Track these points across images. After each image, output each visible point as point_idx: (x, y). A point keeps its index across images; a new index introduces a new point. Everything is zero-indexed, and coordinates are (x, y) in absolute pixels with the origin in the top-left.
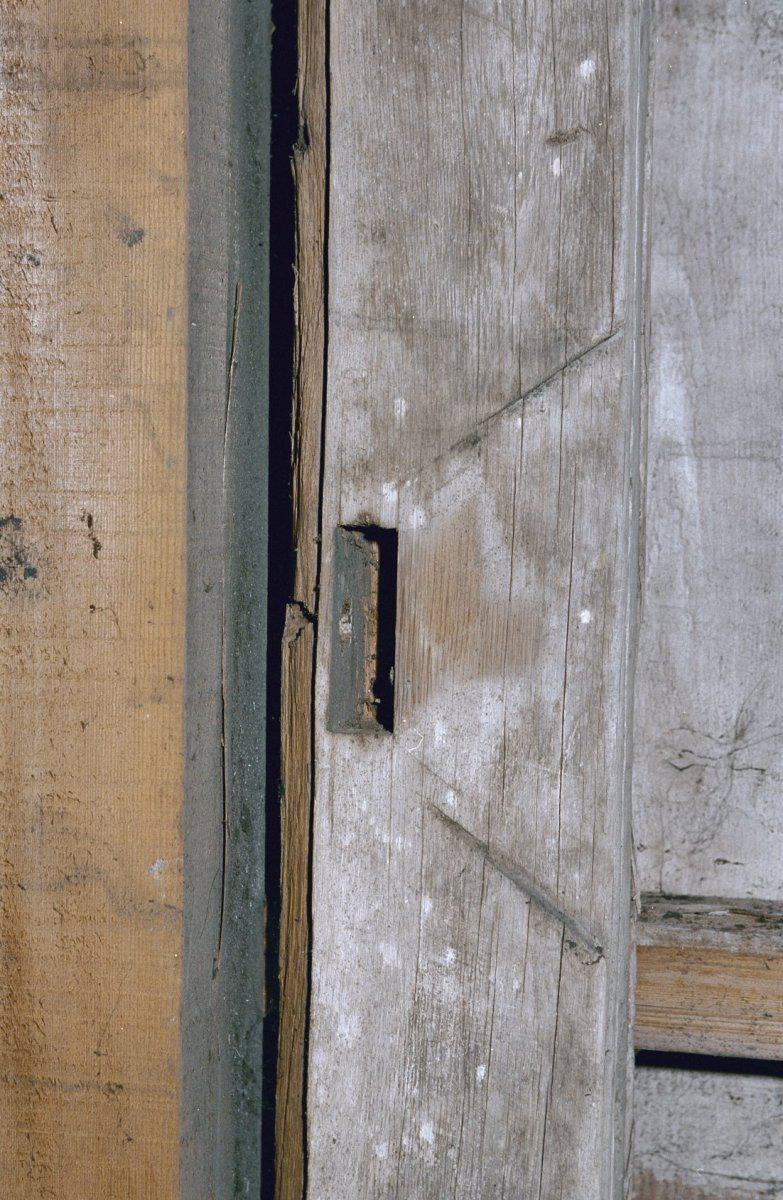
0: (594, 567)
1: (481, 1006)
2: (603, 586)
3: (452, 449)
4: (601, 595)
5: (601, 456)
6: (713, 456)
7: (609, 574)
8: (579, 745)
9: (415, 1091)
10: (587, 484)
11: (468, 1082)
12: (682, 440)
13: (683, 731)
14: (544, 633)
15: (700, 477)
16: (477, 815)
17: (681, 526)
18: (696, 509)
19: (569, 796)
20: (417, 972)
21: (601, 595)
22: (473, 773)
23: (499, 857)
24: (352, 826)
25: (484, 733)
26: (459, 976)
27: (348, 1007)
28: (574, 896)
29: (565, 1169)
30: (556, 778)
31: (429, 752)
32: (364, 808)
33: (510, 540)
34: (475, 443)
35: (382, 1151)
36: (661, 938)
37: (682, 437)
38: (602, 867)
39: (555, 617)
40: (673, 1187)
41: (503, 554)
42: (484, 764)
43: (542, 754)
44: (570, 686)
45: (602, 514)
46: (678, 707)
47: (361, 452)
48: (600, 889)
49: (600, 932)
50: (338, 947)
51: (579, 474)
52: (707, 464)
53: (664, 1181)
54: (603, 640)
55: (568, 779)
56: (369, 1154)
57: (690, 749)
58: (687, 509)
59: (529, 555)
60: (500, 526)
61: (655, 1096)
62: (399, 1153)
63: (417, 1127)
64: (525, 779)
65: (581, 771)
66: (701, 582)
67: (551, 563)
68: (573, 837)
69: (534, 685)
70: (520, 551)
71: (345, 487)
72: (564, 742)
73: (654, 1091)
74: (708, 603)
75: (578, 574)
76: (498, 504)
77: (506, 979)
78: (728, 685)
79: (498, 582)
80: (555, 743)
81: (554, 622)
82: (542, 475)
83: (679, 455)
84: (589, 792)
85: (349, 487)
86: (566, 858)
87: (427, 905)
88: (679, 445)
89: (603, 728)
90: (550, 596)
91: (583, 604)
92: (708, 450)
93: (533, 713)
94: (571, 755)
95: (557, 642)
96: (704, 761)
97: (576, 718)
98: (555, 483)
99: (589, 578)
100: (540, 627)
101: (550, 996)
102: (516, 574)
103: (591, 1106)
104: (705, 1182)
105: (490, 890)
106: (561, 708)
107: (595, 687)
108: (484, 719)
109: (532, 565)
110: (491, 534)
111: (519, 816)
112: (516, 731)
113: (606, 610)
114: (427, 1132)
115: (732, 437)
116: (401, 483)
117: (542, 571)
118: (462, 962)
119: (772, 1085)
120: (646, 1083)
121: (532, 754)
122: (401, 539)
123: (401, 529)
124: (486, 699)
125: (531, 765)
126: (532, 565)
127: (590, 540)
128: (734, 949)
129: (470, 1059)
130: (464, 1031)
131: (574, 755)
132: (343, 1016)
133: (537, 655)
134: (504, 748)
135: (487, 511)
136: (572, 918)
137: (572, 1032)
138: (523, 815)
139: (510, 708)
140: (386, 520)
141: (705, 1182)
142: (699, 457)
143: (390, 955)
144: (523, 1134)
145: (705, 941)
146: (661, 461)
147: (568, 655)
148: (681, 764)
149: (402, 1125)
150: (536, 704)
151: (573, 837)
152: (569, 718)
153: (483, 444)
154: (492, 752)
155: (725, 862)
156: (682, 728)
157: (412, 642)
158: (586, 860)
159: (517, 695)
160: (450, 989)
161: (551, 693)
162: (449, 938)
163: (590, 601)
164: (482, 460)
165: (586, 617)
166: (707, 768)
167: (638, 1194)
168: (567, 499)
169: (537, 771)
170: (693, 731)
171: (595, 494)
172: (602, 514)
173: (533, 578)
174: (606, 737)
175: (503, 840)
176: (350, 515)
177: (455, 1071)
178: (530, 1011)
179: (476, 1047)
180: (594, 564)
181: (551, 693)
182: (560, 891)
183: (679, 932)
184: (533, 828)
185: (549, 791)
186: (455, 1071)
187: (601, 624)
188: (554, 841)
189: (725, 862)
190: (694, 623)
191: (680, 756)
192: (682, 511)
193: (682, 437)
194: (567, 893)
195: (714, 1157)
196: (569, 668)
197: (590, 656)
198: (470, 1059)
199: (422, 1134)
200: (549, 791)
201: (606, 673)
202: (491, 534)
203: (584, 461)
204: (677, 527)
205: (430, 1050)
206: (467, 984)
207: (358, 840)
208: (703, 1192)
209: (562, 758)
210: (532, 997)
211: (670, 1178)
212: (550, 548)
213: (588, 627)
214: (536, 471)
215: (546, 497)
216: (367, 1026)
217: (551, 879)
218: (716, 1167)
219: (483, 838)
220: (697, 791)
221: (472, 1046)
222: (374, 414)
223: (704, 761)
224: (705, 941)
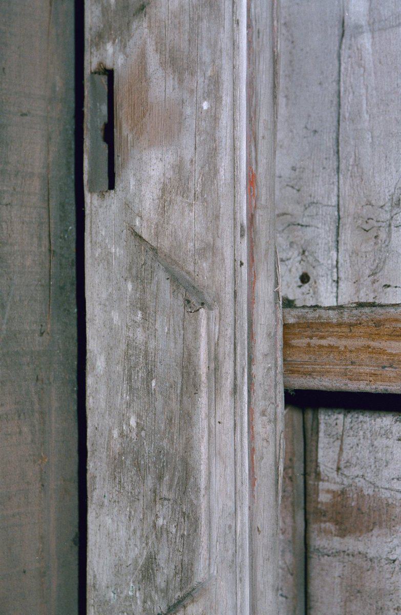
0: (209, 75)
1: (152, 345)
2: (214, 85)
3: (134, 15)
4: (213, 91)
5: (211, 6)
6: (379, 29)
7: (218, 78)
8: (203, 185)
9: (128, 397)
10: (204, 25)
11: (149, 391)
12: (363, 23)
13: (368, 206)
14: (184, 118)
15: (373, 44)
16: (150, 230)
17: (364, 78)
18: (371, 65)
19: (199, 216)
20: (127, 327)
21: (213, 91)
22: (148, 205)
23: (163, 256)
24: (99, 245)
25: (152, 181)
26: (143, 327)
27: (100, 350)
28: (203, 277)
29: (189, 440)
30: (192, 205)
31: (128, 196)
32: (103, 233)
33: (162, 64)
34: (143, 9)
35: (115, 433)
36: (298, 317)
37: (363, 22)
38: (218, 258)
39: (189, 108)
40: (372, 499)
41: (160, 74)
42: (153, 200)
43: (184, 191)
44: (199, 149)
45: (213, 41)
46: (365, 191)
47: (98, 28)
48: (217, 273)
49: (219, 298)
50: (96, 316)
51: (200, 19)
52: (376, 34)
53: (368, 495)
54: (216, 119)
55: (198, 207)
56: (110, 436)
57: (371, 217)
58: (367, 66)
59: (174, 72)
60: (158, 56)
61: (362, 441)
62: (121, 435)
63: (129, 418)
64: (176, 207)
65: (205, 200)
66: (375, 110)
67: (186, 75)
68: (202, 241)
69: (179, 150)
70: (170, 70)
71: (92, 50)
72: (196, 184)
73: (362, 437)
74: (379, 123)
75: (201, 80)
76: (156, 43)
77: (161, 325)
78: (390, 173)
79: (157, 90)
80: (191, 185)
81: (188, 111)
82: (179, 23)
83: (362, 33)
84: (210, 212)
85: (94, 49)
86: (199, 254)
87: (130, 286)
88: (361, 27)
89: (216, 172)
90: (186, 95)
91: (204, 98)
92: (376, 26)
93: (179, 168)
94: (200, 191)
95: (191, 123)
96: (379, 224)
97: (202, 168)
98: (187, 26)
99: (206, 81)
100: (181, 114)
101: (180, 335)
102: (168, 84)
103: (198, 400)
104: (389, 495)
105: (155, 274)
106: (194, 162)
107: (212, 148)
108: (152, 173)
109: (176, 79)
110: (153, 60)
111: (173, 230)
112: (170, 179)
113: (217, 100)
114: (133, 422)
115: (389, 15)
116: (114, 41)
117: (181, 81)
118: (145, 319)
119: (387, 421)
120: (357, 432)
121: (179, 192)
122: (115, 74)
123: (115, 68)
124: (154, 161)
125: (179, 198)
126: (176, 79)
127: (207, 58)
128: (335, 321)
129: (150, 374)
130: (146, 360)
131: (202, 191)
132: (98, 356)
133: (180, 131)
134: (163, 190)
135: (151, 48)
136: (202, 290)
137: (190, 355)
138: (175, 230)
139: (167, 165)
140: (109, 65)
141: (389, 495)
142: (372, 31)
143: (116, 317)
144: (171, 420)
145: (320, 317)
146: (353, 39)
147: (197, 130)
148: (367, 227)
149: (123, 419)
150: (181, 161)
151: (202, 241)
152: (198, 169)
153: (147, 9)
154: (157, 192)
155: (389, 286)
156: (367, 205)
157: (120, 133)
158: (209, 254)
159: (170, 158)
160: (140, 335)
161: (188, 154)
162: (139, 305)
163: (207, 95)
164: (147, 19)
165: (205, 105)
166: (381, 228)
167: (356, 503)
168: (194, 33)
169: (182, 202)
170: (373, 206)
171: (209, 30)
172: (213, 41)
173: (177, 86)
174: (218, 178)
175: (165, 244)
176: (94, 66)
177: (144, 385)
178: (172, 345)
179: (151, 369)
180: (209, 73)
181: (188, 154)
182: (196, 275)
183: (307, 313)
184: (181, 237)
185: (189, 214)
186: (144, 385)
187: (214, 109)
188: (192, 244)
189: (389, 286)
190: (372, 137)
191: (367, 222)
192: (364, 68)
193: (363, 22)
194: (200, 276)
195: (393, 479)
196: (197, 138)
197: (208, 128)
198: (150, 374)
199: (131, 423)
200: (189, 214)
201: (217, 139)
202: (153, 60)
203: (202, 11)
204: (362, 78)
205: (133, 373)
206: (147, 332)
207: (101, 253)
208: (388, 502)
209: (195, 194)
210: (172, 337)
211: (371, 493)
212: (185, 66)
213: (207, 111)
214: (177, 21)
215: (182, 36)
216: (108, 360)
217: (191, 268)
218: (395, 486)
219: (154, 244)
220: (376, 244)
221: (150, 369)
222: (103, 5)
223: (379, 224)
224: (320, 317)
